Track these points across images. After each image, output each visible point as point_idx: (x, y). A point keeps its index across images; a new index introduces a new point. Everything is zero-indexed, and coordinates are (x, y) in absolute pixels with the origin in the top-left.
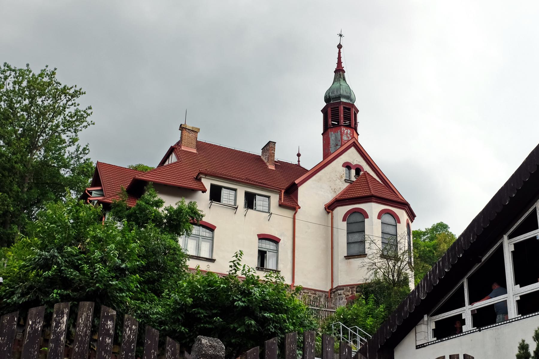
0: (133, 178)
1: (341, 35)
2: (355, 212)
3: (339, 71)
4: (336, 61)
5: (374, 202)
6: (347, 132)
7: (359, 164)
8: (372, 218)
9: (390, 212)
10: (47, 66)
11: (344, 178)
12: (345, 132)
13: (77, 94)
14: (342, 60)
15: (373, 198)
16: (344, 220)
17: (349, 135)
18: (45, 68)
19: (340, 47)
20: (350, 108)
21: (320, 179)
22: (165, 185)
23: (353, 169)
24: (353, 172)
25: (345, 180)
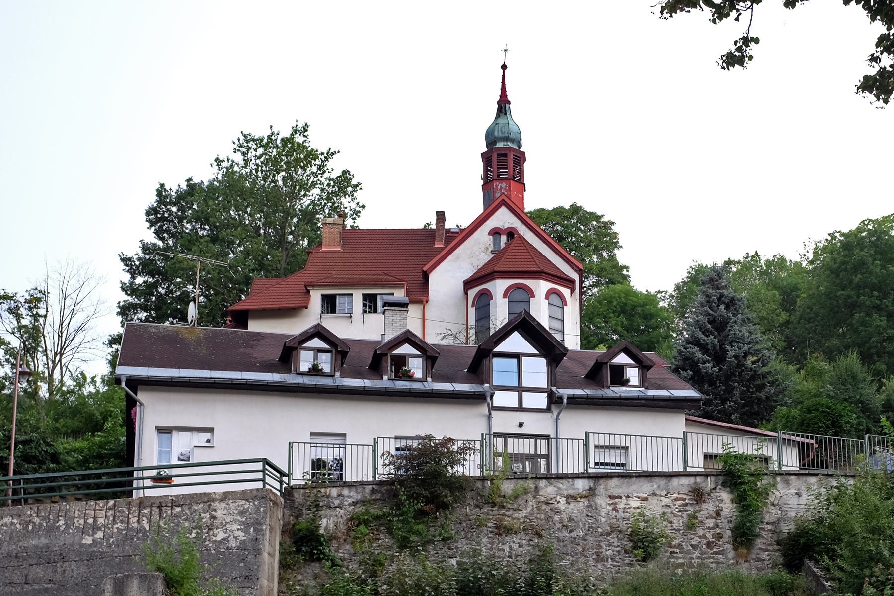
0: (303, 283)
1: (506, 51)
2: (482, 294)
3: (503, 105)
4: (500, 87)
5: (498, 278)
6: (501, 186)
7: (512, 226)
8: (496, 298)
9: (522, 287)
10: (297, 121)
11: (490, 249)
12: (499, 187)
13: (330, 154)
14: (507, 86)
15: (495, 274)
16: (505, 296)
17: (505, 189)
18: (296, 123)
19: (504, 67)
20: (507, 154)
21: (458, 258)
22: (264, 310)
23: (503, 235)
24: (504, 238)
25: (491, 251)
